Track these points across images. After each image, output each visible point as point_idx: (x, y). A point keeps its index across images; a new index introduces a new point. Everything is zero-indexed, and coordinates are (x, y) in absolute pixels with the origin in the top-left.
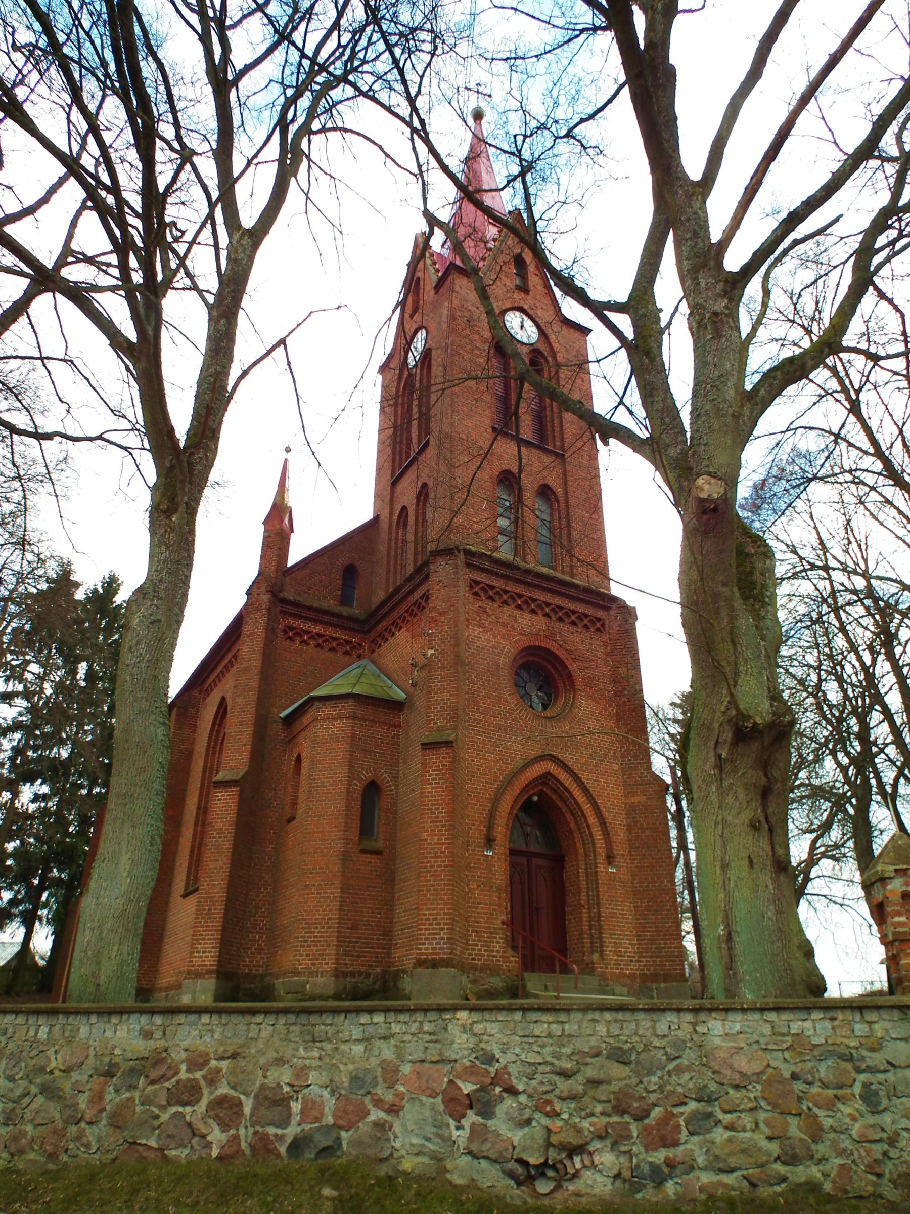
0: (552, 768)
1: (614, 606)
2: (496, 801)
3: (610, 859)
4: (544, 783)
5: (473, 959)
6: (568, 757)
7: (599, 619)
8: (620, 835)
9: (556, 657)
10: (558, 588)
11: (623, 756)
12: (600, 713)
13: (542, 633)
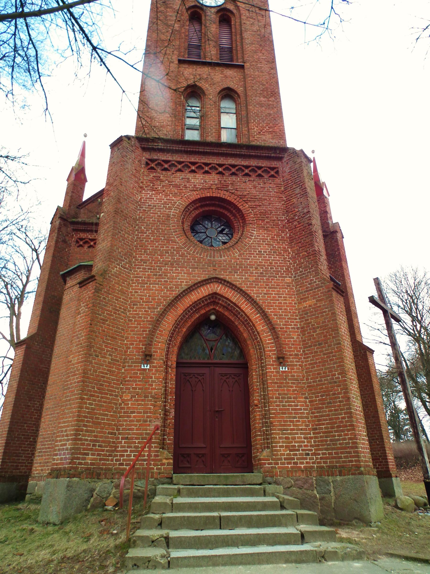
0: (218, 288)
1: (286, 155)
2: (157, 323)
3: (281, 360)
4: (214, 303)
5: (122, 464)
6: (236, 278)
7: (273, 169)
8: (293, 337)
9: (230, 203)
10: (229, 151)
11: (296, 270)
12: (273, 238)
13: (214, 187)
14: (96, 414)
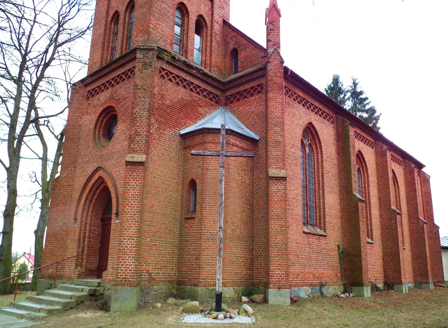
14: (54, 251)
